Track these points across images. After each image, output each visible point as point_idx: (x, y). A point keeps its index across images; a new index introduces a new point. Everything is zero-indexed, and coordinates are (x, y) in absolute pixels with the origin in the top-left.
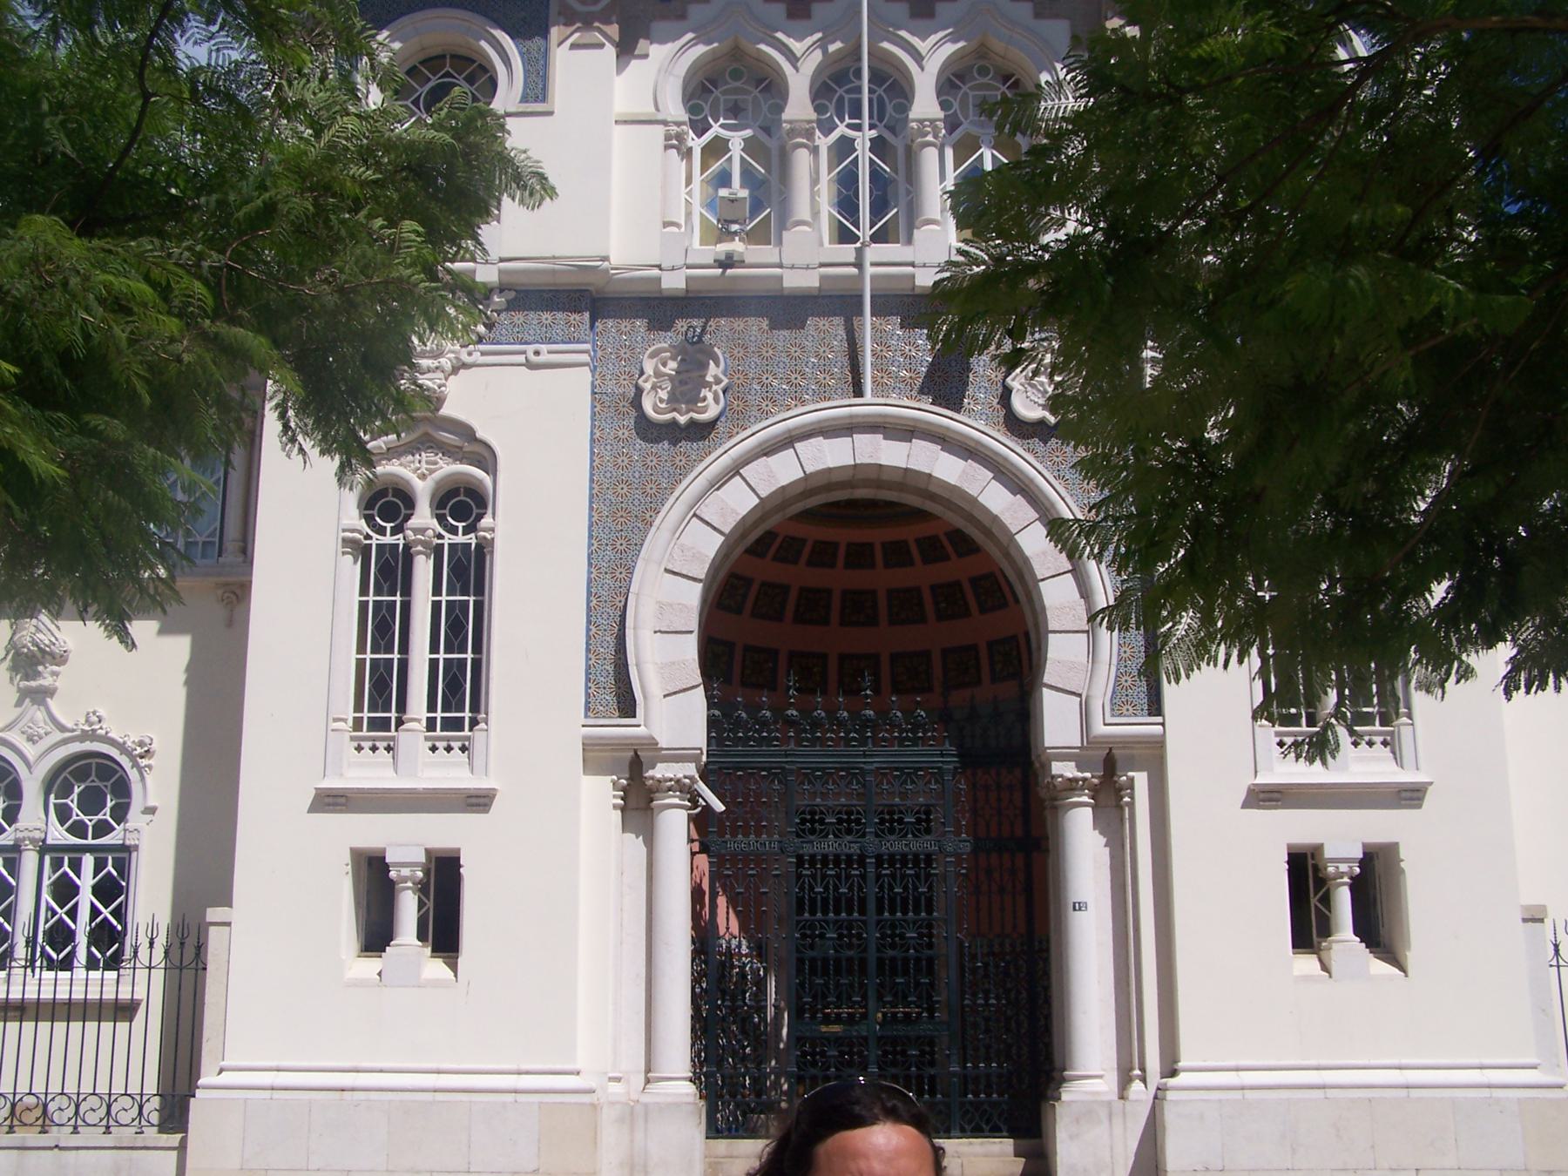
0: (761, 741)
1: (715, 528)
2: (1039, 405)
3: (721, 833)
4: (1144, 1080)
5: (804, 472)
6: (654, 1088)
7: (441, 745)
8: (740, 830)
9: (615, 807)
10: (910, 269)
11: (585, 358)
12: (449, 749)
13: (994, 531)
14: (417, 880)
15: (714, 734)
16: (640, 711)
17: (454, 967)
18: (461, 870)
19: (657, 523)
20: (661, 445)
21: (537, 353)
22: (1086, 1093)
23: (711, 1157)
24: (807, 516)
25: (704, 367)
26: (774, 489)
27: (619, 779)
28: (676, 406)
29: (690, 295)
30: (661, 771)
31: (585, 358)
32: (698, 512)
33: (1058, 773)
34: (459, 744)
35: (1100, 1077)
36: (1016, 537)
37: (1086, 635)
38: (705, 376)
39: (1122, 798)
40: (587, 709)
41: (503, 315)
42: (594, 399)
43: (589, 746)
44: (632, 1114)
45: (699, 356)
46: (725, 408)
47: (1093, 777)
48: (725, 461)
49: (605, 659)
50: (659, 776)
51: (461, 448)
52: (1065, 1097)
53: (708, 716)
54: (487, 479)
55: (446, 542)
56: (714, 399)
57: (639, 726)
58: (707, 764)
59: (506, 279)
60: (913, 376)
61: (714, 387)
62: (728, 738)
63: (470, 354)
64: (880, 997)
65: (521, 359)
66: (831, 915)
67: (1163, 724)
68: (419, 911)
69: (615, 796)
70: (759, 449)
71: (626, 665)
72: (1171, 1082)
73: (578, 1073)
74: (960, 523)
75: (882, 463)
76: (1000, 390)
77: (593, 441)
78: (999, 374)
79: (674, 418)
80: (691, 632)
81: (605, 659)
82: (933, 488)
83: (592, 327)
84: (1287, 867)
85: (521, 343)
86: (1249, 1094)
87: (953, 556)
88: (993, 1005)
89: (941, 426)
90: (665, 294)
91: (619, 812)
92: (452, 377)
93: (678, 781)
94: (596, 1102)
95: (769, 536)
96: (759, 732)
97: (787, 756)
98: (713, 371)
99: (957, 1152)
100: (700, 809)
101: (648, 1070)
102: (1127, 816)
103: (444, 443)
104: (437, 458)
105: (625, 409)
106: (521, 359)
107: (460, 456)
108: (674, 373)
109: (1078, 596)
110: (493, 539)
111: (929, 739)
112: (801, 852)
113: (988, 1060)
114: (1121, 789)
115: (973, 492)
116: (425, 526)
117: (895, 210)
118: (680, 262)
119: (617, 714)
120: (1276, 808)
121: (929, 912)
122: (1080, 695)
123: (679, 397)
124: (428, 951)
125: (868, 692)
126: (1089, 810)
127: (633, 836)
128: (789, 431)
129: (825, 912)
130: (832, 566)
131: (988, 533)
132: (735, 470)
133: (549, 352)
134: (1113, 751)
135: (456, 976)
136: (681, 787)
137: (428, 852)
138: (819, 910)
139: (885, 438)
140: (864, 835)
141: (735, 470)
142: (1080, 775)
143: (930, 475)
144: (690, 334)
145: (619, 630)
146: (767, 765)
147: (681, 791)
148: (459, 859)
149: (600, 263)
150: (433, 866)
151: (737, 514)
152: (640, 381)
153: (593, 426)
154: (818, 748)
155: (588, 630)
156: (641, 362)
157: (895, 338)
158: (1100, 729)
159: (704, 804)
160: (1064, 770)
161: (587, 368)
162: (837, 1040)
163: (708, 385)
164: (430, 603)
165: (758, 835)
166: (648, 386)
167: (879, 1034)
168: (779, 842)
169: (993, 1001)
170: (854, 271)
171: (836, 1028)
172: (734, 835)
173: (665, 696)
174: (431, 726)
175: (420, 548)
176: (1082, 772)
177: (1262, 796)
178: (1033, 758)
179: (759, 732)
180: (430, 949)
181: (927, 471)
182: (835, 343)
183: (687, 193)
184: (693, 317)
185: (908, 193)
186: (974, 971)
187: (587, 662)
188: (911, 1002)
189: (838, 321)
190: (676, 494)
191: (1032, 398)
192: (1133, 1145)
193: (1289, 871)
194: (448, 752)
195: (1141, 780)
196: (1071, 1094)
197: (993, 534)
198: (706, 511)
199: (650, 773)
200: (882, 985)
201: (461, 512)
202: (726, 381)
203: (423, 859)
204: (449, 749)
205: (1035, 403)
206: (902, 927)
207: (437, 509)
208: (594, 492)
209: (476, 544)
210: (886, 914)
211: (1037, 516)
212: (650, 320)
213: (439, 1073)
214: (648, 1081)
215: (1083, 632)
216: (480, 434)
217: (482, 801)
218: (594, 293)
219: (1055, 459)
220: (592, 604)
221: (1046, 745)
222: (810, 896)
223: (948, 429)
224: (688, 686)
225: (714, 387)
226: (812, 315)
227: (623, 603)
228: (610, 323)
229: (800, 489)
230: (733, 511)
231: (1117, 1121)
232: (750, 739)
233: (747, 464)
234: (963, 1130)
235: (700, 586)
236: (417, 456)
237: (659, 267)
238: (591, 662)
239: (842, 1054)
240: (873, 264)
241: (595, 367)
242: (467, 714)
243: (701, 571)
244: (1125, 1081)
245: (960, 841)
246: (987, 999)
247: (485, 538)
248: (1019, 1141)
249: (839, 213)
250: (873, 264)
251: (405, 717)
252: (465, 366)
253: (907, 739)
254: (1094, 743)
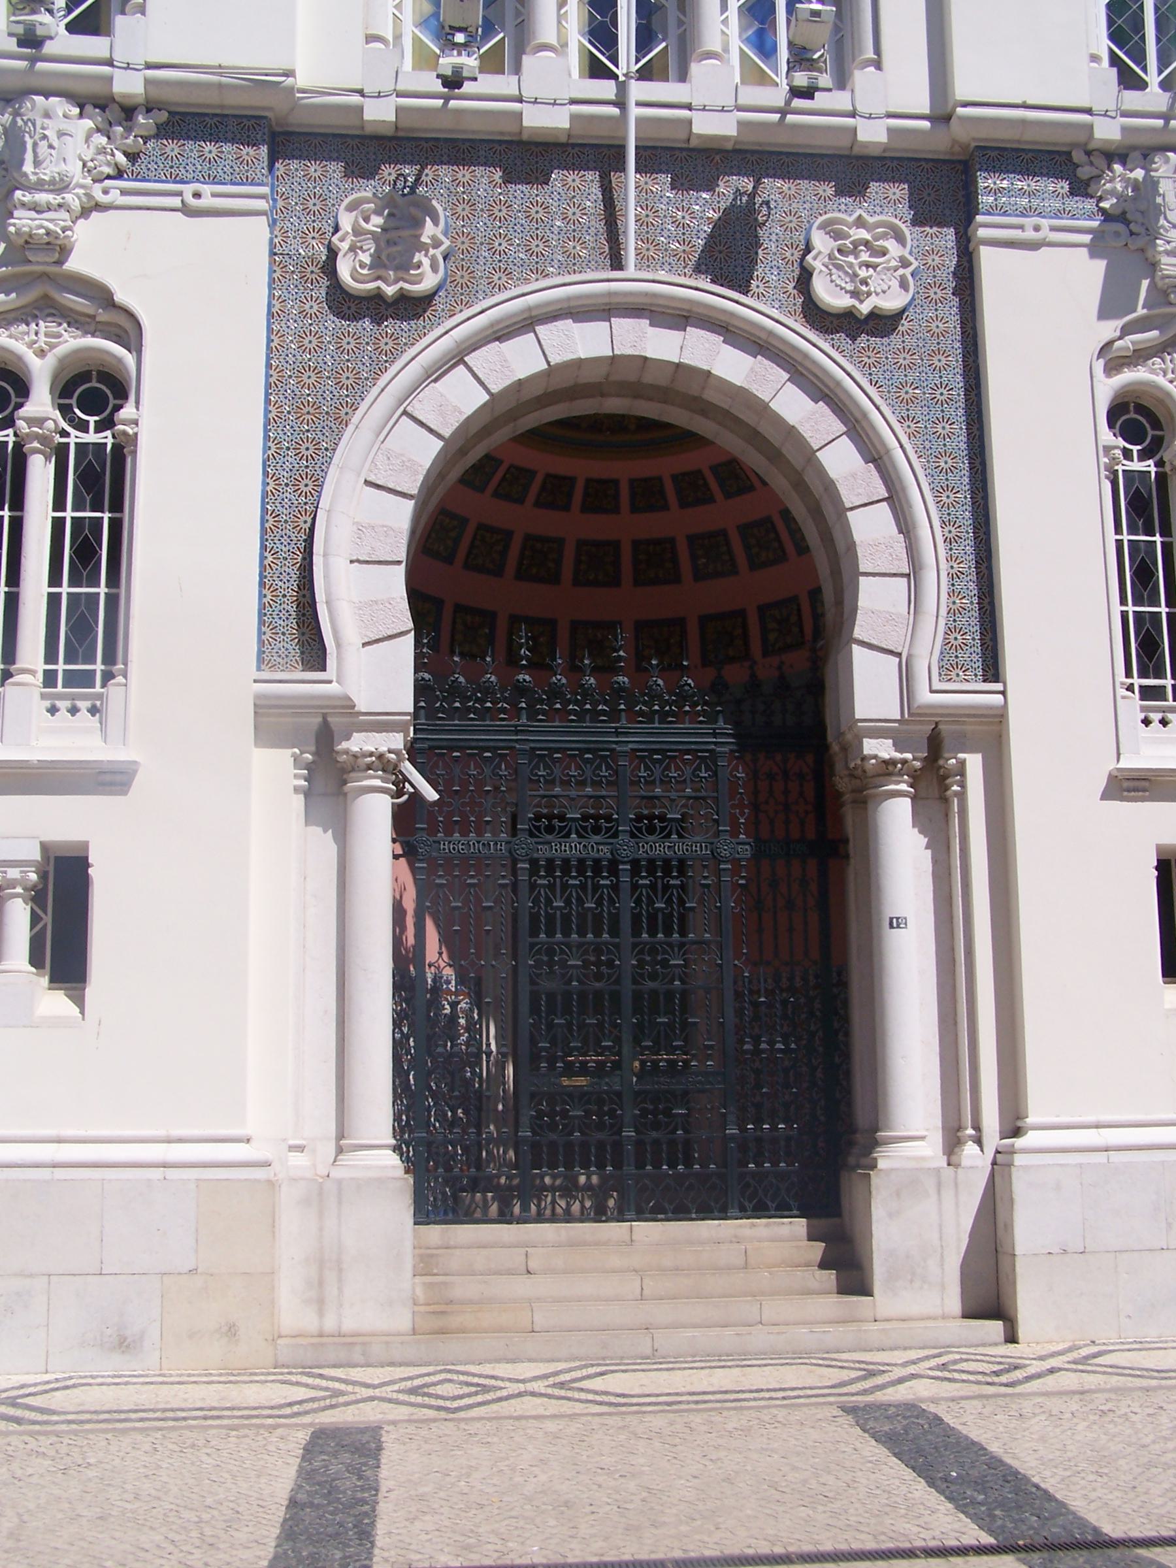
0: (483, 714)
1: (431, 431)
2: (846, 292)
3: (432, 831)
4: (979, 1141)
5: (548, 363)
6: (347, 1158)
7: (63, 705)
8: (457, 827)
9: (297, 790)
10: (685, 113)
11: (262, 205)
12: (74, 711)
13: (784, 451)
14: (30, 884)
15: (422, 704)
16: (331, 662)
17: (80, 1001)
18: (90, 871)
19: (355, 420)
20: (360, 323)
21: (197, 195)
22: (909, 1158)
23: (420, 1248)
24: (537, 437)
25: (419, 224)
26: (508, 382)
27: (302, 753)
28: (381, 272)
29: (401, 134)
30: (359, 743)
31: (262, 205)
32: (409, 409)
33: (871, 753)
34: (88, 704)
35: (922, 1138)
36: (818, 454)
37: (905, 580)
38: (420, 235)
39: (947, 788)
40: (260, 660)
41: (151, 144)
42: (272, 262)
43: (264, 709)
44: (321, 1194)
45: (413, 210)
46: (444, 280)
47: (914, 759)
48: (446, 343)
49: (284, 596)
50: (355, 749)
51: (93, 317)
52: (881, 1164)
53: (416, 680)
54: (129, 359)
55: (72, 441)
56: (431, 266)
57: (330, 682)
58: (415, 740)
59: (155, 93)
60: (687, 249)
61: (432, 252)
62: (442, 709)
63: (106, 192)
64: (637, 1041)
65: (176, 202)
66: (574, 936)
67: (1003, 693)
68: (31, 929)
69: (296, 776)
70: (490, 331)
71: (313, 604)
72: (1019, 1142)
73: (248, 1141)
74: (732, 444)
75: (648, 356)
76: (797, 272)
77: (270, 315)
78: (796, 252)
79: (379, 288)
80: (399, 562)
81: (284, 596)
82: (710, 395)
83: (271, 167)
84: (1156, 873)
85: (175, 182)
86: (1115, 1157)
87: (719, 495)
88: (763, 1051)
89: (724, 311)
90: (369, 130)
91: (302, 797)
92: (81, 221)
93: (381, 757)
94: (274, 1179)
95: (488, 463)
96: (481, 701)
97: (517, 732)
98: (429, 230)
99: (736, 1237)
100: (405, 797)
101: (341, 1135)
102: (956, 810)
103: (71, 310)
104: (61, 329)
105: (314, 276)
106: (176, 202)
107: (92, 328)
108: (379, 230)
109: (896, 531)
110: (136, 434)
111: (698, 714)
112: (535, 855)
113: (758, 1122)
114: (945, 777)
115: (764, 396)
116: (44, 415)
117: (663, 45)
118: (388, 86)
119: (300, 667)
120: (1143, 800)
121: (683, 933)
122: (899, 655)
123: (386, 261)
124: (45, 981)
125: (622, 653)
126: (907, 802)
127: (319, 830)
128: (530, 309)
129: (566, 933)
130: (566, 508)
131: (775, 455)
132: (458, 358)
133: (214, 195)
134: (941, 727)
135: (82, 1012)
136: (383, 764)
137: (45, 847)
138: (558, 931)
139: (651, 325)
140: (615, 835)
141: (458, 358)
142: (898, 755)
143: (709, 372)
144: (400, 185)
145: (304, 559)
146: (491, 744)
147: (384, 770)
148: (87, 858)
149: (283, 79)
150: (51, 869)
151: (461, 413)
152: (335, 239)
153: (271, 296)
154: (557, 724)
155: (262, 558)
156: (336, 217)
157: (664, 200)
158: (925, 697)
159: (412, 790)
160: (879, 748)
161: (264, 218)
162: (581, 1097)
163: (424, 248)
164: (50, 520)
165: (480, 834)
166: (345, 246)
167: (636, 1088)
168: (507, 843)
169: (780, 1046)
170: (615, 111)
171: (581, 1081)
172: (449, 833)
173: (364, 645)
174: (50, 679)
175: (36, 444)
176: (902, 753)
177: (1126, 784)
178: (830, 738)
179: (481, 701)
180: (47, 978)
181: (705, 368)
182: (588, 203)
183: (396, 7)
184: (404, 162)
185: (681, 23)
186: (756, 1005)
187: (260, 599)
188: (677, 1048)
189: (592, 176)
190: (381, 383)
191: (838, 282)
192: (967, 1222)
193: (1158, 878)
194: (73, 715)
195: (974, 763)
196: (888, 1159)
197: (784, 456)
198: (419, 408)
199: (344, 745)
200: (640, 1026)
201: (93, 403)
202: (447, 243)
203: (37, 856)
204: (74, 711)
205: (842, 289)
206: (665, 952)
207: (60, 397)
208: (271, 380)
209: (113, 444)
210: (645, 935)
211: (845, 429)
212: (347, 163)
213: (59, 1141)
214: (340, 1150)
215: (902, 575)
216: (120, 297)
217: (118, 778)
218: (274, 124)
219: (866, 359)
220: (267, 525)
221: (857, 717)
222: (546, 912)
223: (732, 314)
224: (395, 632)
225: (432, 252)
226: (559, 167)
227: (308, 525)
228: (294, 164)
229: (538, 391)
230: (456, 409)
231: (948, 1195)
232: (469, 710)
233: (474, 350)
234: (742, 1209)
235: (411, 504)
236: (33, 325)
237: (361, 92)
238: (265, 600)
239: (588, 1114)
240: (639, 104)
241: (275, 221)
242: (99, 667)
243: (413, 485)
244: (952, 1144)
245: (738, 844)
246: (771, 1043)
247: (125, 433)
248: (815, 1222)
249: (590, 42)
250: (639, 104)
251: (13, 668)
252: (99, 207)
253: (671, 713)
254: (920, 715)
